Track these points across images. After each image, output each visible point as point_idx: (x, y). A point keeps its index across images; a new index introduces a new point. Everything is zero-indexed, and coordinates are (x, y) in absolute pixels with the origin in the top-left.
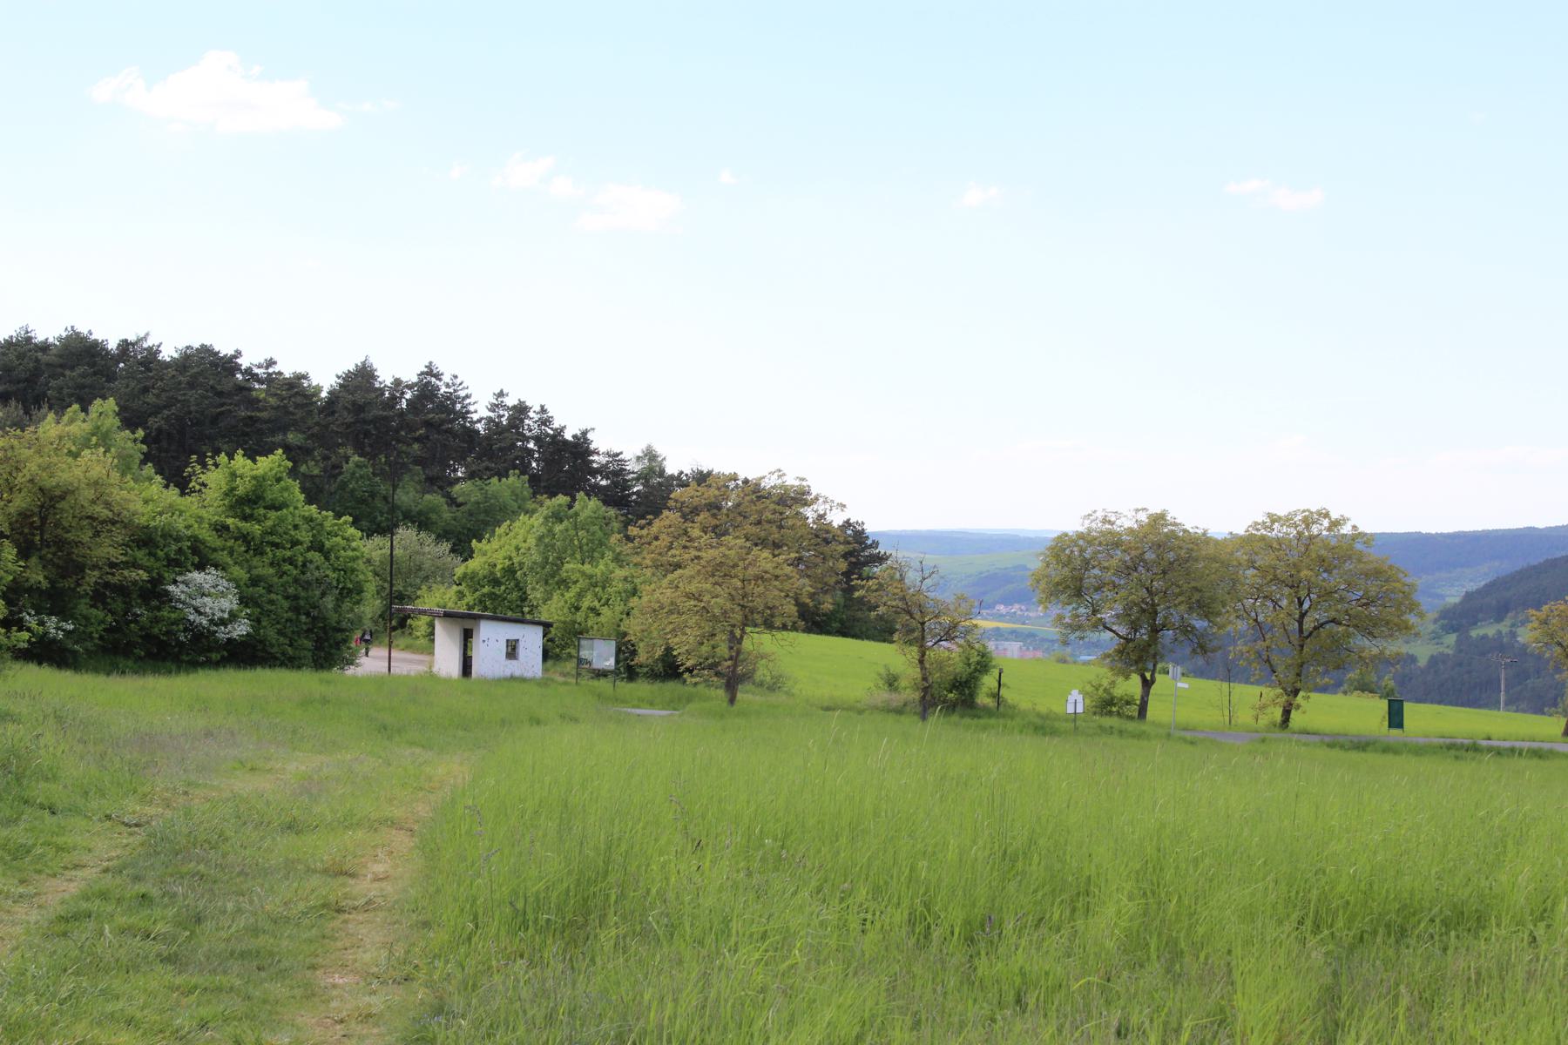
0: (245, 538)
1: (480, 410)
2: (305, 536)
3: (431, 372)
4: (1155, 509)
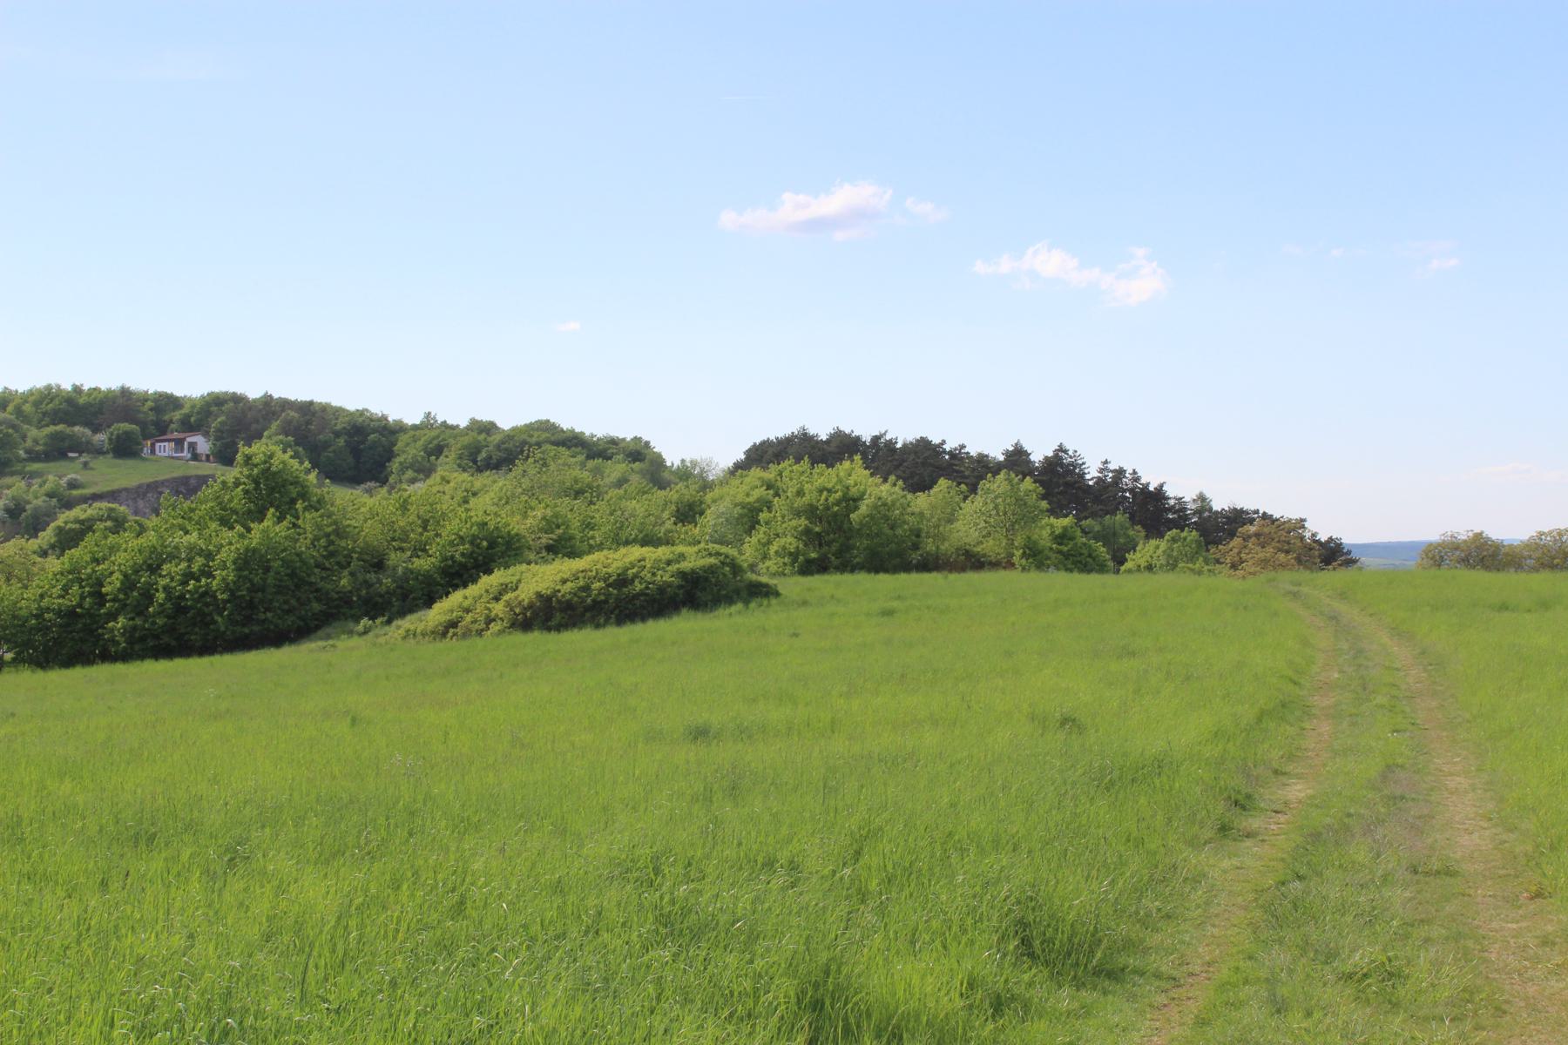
0: (1060, 552)
1: (1092, 473)
2: (1085, 552)
3: (1061, 449)
4: (1477, 530)
